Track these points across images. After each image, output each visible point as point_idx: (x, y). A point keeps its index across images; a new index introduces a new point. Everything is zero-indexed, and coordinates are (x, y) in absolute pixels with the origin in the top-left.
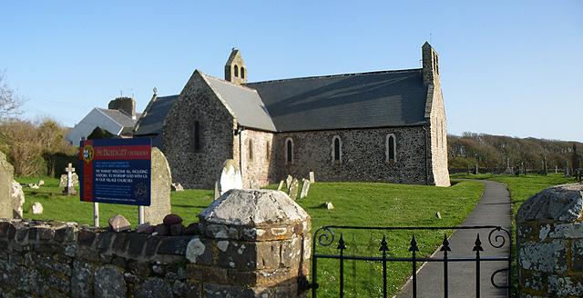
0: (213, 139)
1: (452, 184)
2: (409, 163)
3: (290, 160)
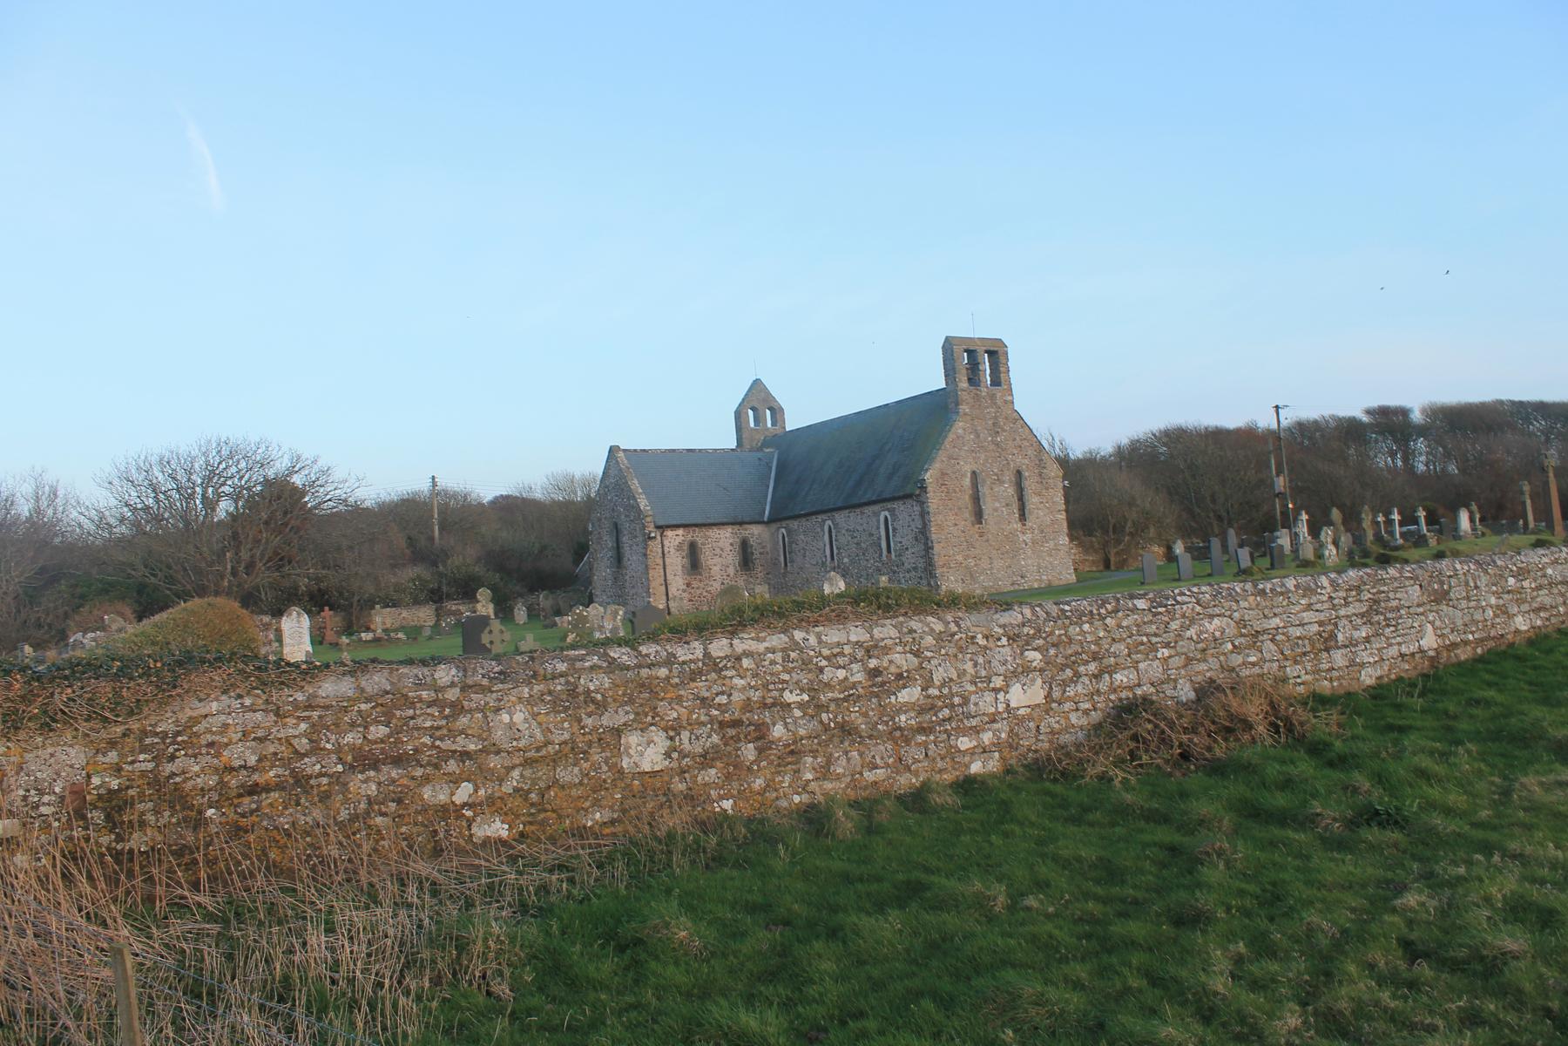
0: (631, 546)
1: (1078, 581)
3: (786, 565)
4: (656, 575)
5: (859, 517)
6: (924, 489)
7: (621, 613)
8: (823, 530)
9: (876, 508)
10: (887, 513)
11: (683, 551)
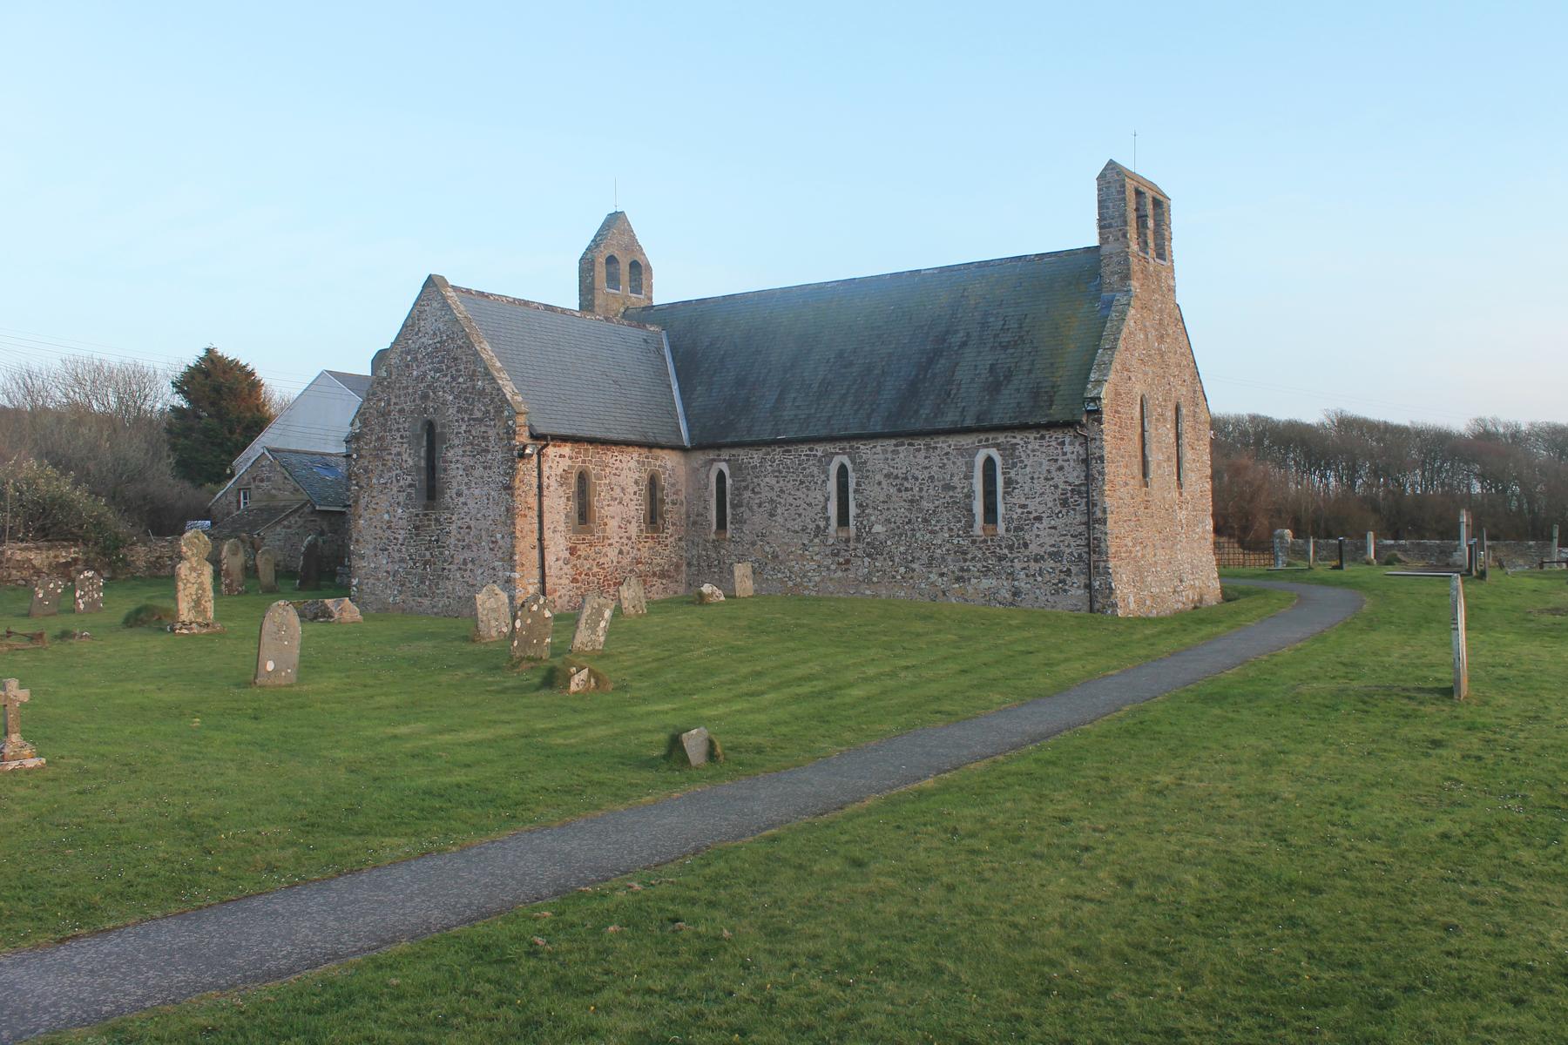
0: (468, 470)
1: (1227, 597)
2: (1041, 538)
3: (722, 524)
4: (526, 526)
5: (923, 453)
6: (1096, 415)
8: (826, 473)
9: (966, 441)
10: (994, 453)
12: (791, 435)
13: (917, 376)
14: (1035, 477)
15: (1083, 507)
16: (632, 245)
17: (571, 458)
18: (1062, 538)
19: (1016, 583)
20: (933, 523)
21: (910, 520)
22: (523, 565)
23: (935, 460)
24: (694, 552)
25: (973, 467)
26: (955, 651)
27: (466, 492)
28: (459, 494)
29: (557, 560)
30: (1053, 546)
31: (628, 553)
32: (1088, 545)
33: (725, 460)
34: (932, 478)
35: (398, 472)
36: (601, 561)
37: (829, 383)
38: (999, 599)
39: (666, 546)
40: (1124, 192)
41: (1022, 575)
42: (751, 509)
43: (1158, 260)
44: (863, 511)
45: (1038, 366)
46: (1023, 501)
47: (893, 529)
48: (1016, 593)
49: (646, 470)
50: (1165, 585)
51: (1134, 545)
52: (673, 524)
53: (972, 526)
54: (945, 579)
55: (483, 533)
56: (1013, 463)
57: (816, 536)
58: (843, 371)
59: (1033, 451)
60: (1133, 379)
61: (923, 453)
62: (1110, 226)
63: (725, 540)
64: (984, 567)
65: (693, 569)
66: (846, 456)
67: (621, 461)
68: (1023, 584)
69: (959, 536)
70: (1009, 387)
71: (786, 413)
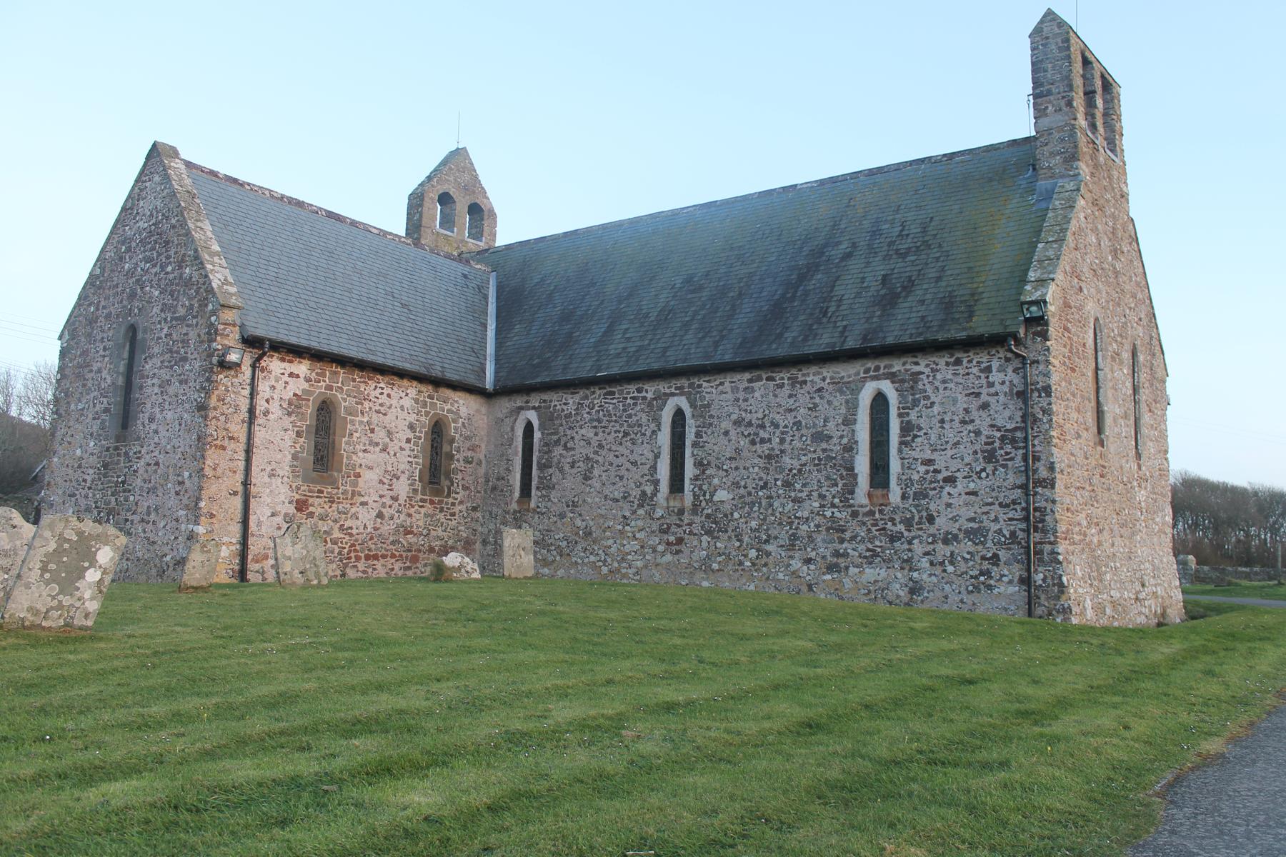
0: (164, 384)
1: (1193, 613)
5: (787, 390)
6: (1038, 323)
7: (105, 555)
9: (847, 371)
10: (887, 387)
11: (302, 416)
12: (615, 370)
13: (783, 295)
14: (947, 418)
15: (1018, 462)
16: (474, 185)
17: (308, 380)
18: (986, 509)
19: (915, 575)
20: (798, 486)
21: (766, 484)
22: (212, 516)
23: (803, 399)
24: (492, 526)
25: (856, 407)
26: (803, 671)
27: (159, 416)
28: (151, 420)
29: (273, 515)
30: (972, 520)
31: (392, 518)
32: (1027, 519)
33: (534, 408)
34: (798, 424)
35: (96, 393)
36: (347, 524)
37: (670, 311)
38: (890, 598)
39: (453, 515)
40: (1068, 48)
41: (924, 563)
42: (561, 470)
43: (1108, 151)
44: (703, 472)
45: (949, 272)
46: (928, 455)
47: (743, 497)
48: (915, 589)
49: (427, 413)
50: (1126, 589)
51: (1089, 527)
52: (465, 488)
53: (852, 492)
54: (813, 567)
55: (171, 470)
56: (914, 400)
57: (641, 506)
58: (690, 296)
59: (944, 382)
60: (1085, 291)
61: (787, 390)
62: (1049, 93)
63: (528, 510)
64: (868, 550)
65: (489, 547)
66: (683, 398)
67: (389, 396)
68: (925, 576)
69: (833, 506)
70: (910, 299)
71: (612, 346)
